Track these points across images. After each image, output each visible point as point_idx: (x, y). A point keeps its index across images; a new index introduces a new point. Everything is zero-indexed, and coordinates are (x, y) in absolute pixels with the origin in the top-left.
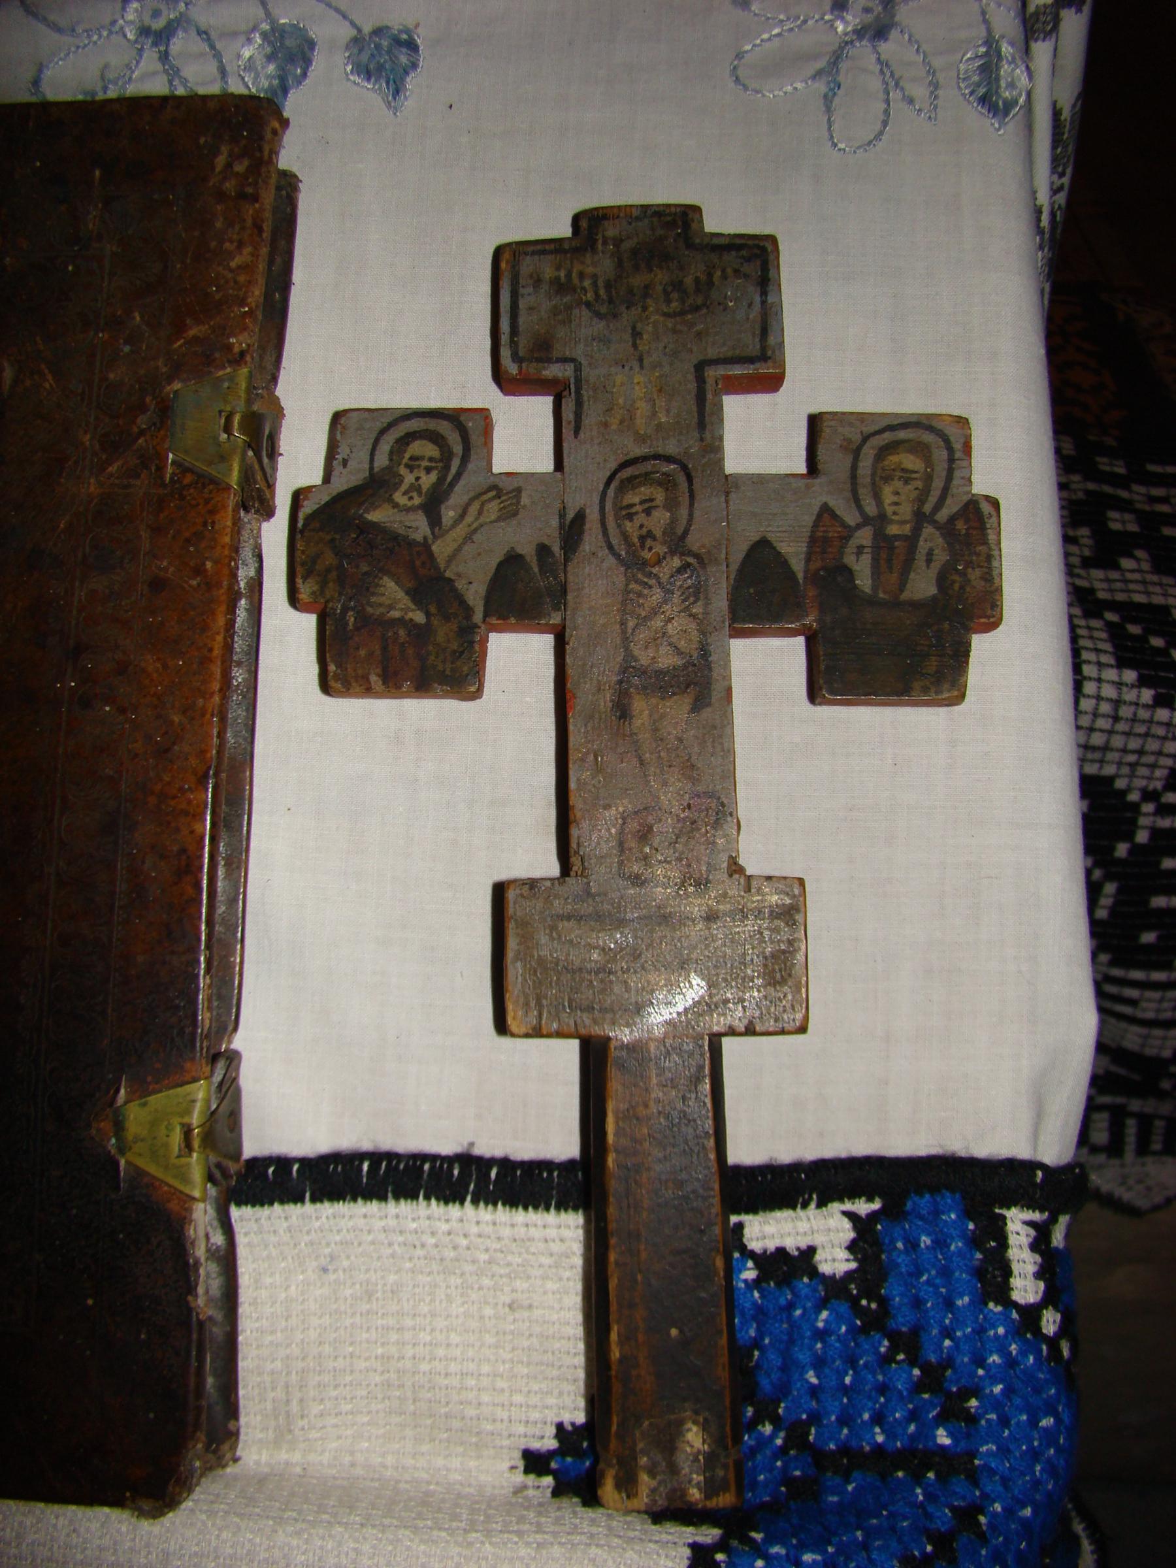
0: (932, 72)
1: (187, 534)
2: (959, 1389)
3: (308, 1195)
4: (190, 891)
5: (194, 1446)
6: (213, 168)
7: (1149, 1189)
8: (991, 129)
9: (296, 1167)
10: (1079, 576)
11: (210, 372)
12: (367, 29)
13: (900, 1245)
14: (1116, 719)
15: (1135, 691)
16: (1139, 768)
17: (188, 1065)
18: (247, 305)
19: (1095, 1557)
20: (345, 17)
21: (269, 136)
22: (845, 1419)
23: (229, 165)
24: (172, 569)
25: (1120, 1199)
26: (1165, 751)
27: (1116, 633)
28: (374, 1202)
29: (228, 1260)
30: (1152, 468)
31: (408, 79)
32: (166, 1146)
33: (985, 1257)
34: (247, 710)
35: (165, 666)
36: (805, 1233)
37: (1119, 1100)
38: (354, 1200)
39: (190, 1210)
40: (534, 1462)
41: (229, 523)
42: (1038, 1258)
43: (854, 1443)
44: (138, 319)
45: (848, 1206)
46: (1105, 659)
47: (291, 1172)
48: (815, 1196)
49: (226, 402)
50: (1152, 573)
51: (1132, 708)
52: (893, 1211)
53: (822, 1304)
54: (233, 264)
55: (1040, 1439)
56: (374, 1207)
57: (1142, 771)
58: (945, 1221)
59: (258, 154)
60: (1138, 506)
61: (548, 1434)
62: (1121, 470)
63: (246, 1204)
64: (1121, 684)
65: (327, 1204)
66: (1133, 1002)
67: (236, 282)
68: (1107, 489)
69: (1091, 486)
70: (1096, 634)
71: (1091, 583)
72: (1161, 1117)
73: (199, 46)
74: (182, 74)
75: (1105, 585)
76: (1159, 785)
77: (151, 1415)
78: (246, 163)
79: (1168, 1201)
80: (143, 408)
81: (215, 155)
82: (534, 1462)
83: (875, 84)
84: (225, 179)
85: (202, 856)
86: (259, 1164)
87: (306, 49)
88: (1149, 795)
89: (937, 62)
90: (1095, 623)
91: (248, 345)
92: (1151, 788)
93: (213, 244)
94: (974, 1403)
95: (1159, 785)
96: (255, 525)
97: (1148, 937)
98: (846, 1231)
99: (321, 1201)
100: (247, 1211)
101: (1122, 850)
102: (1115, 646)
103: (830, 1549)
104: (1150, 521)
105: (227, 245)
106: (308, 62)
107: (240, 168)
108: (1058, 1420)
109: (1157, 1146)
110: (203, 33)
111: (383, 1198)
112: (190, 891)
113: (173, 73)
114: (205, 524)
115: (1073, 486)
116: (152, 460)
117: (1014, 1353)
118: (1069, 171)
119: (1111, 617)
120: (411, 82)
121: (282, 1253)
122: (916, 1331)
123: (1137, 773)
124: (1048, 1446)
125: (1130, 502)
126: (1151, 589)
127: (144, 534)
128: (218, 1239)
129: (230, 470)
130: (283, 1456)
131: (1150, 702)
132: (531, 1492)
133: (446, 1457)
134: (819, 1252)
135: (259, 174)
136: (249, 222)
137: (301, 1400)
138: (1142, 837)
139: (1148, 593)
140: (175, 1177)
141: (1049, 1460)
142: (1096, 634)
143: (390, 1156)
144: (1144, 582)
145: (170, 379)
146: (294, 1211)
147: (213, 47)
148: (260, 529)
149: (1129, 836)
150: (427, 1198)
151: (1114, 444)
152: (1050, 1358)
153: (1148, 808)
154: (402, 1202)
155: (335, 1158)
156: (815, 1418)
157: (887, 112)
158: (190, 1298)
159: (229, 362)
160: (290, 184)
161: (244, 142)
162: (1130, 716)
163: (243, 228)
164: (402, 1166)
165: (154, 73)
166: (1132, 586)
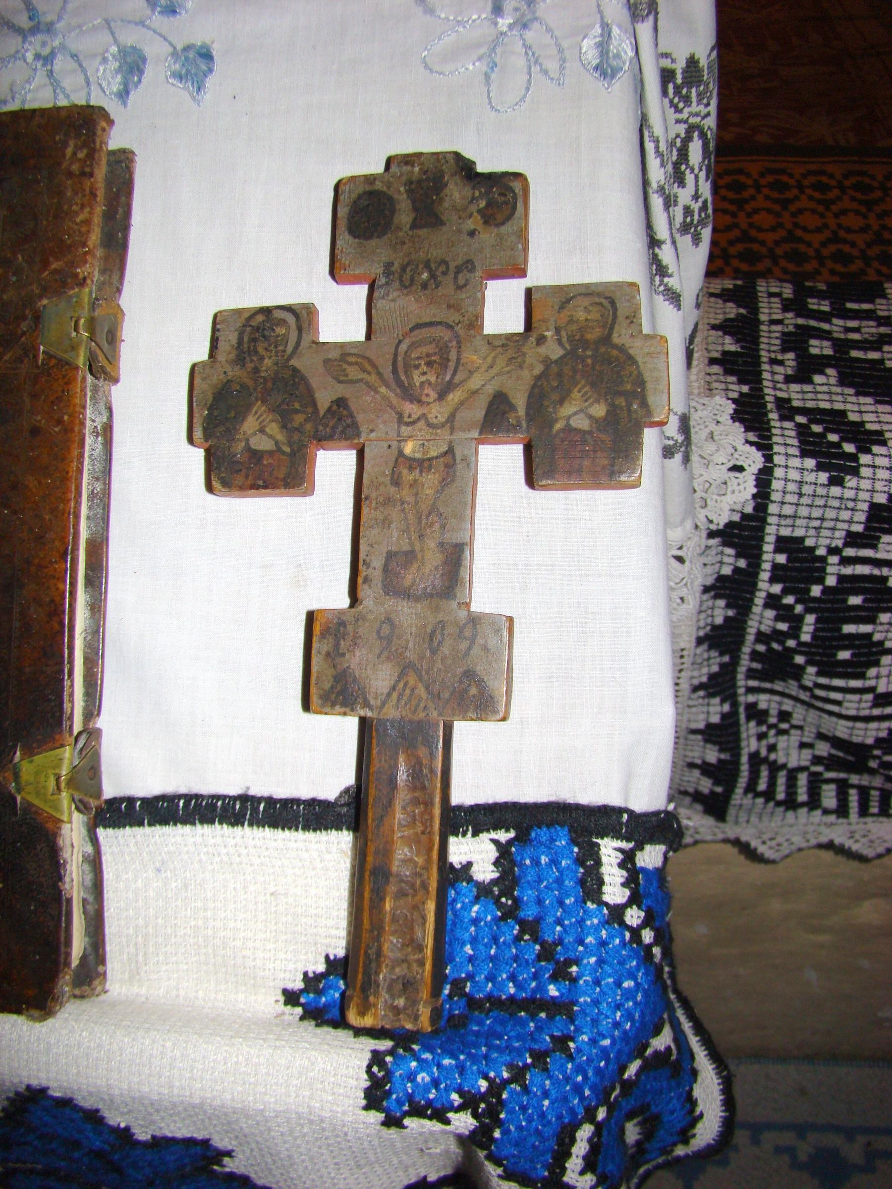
0: (561, 51)
1: (52, 398)
2: (565, 959)
3: (146, 821)
4: (56, 626)
5: (63, 977)
6: (64, 156)
7: (872, 842)
8: (603, 89)
9: (138, 803)
10: (780, 390)
11: (65, 292)
12: (179, 47)
13: (528, 862)
14: (800, 495)
15: (814, 474)
16: (822, 530)
17: (57, 737)
18: (87, 246)
19: (721, 1087)
20: (165, 39)
21: (99, 132)
22: (491, 978)
23: (74, 154)
24: (43, 421)
25: (850, 848)
26: (841, 518)
27: (803, 432)
28: (188, 826)
29: (95, 863)
30: (849, 305)
31: (207, 80)
32: (45, 787)
33: (586, 871)
34: (104, 509)
35: (40, 483)
36: (466, 853)
37: (842, 775)
38: (175, 824)
39: (60, 828)
40: (291, 998)
41: (79, 390)
42: (625, 873)
43: (495, 993)
44: (20, 258)
45: (493, 835)
46: (791, 451)
47: (135, 807)
48: (470, 828)
49: (75, 311)
50: (837, 386)
51: (813, 487)
52: (522, 838)
53: (477, 899)
54: (78, 220)
55: (622, 995)
56: (188, 829)
57: (825, 533)
58: (558, 846)
59: (92, 145)
60: (835, 335)
61: (298, 979)
62: (826, 309)
63: (110, 827)
64: (803, 469)
65: (158, 827)
66: (838, 703)
67: (80, 231)
68: (813, 323)
69: (800, 321)
70: (786, 433)
71: (789, 394)
72: (875, 788)
73: (72, 65)
74: (62, 85)
75: (800, 396)
76: (840, 543)
77: (37, 957)
78: (85, 151)
79: (888, 851)
80: (24, 318)
81: (66, 148)
82: (291, 998)
83: (521, 62)
84: (72, 163)
85: (64, 604)
86: (114, 803)
87: (140, 63)
88: (832, 551)
89: (565, 44)
90: (788, 424)
91: (89, 273)
92: (833, 545)
93: (66, 207)
94: (574, 969)
95: (840, 543)
96: (106, 388)
97: (844, 655)
98: (492, 853)
99: (154, 825)
100: (110, 831)
101: (816, 591)
102: (800, 441)
103: (462, 1057)
104: (841, 346)
105: (74, 207)
106: (141, 72)
107: (81, 155)
108: (637, 984)
109: (875, 810)
110: (74, 56)
111: (193, 823)
112: (56, 626)
113: (56, 85)
114: (63, 391)
115: (786, 322)
116: (30, 351)
117: (604, 936)
118: (714, 103)
119: (801, 419)
120: (210, 82)
121: (132, 859)
122: (538, 920)
123: (821, 534)
124: (627, 999)
125: (829, 332)
126: (834, 398)
127: (27, 399)
128: (89, 849)
129: (78, 355)
130: (135, 989)
131: (826, 483)
132: (287, 1017)
133: (235, 994)
134: (475, 865)
135: (94, 159)
136: (88, 191)
137: (145, 954)
138: (831, 581)
139: (831, 401)
140: (51, 807)
141: (627, 1010)
142: (786, 433)
143: (198, 797)
144: (830, 393)
145: (41, 297)
146: (138, 831)
147: (81, 66)
148: (110, 390)
149: (821, 581)
150: (221, 823)
151: (824, 288)
152: (632, 940)
153: (834, 559)
154: (206, 826)
155: (163, 797)
156: (470, 977)
157: (529, 82)
158: (60, 884)
159: (77, 285)
160: (128, 158)
161: (83, 137)
162: (811, 493)
163: (84, 196)
164: (204, 803)
165: (45, 85)
166: (820, 396)
